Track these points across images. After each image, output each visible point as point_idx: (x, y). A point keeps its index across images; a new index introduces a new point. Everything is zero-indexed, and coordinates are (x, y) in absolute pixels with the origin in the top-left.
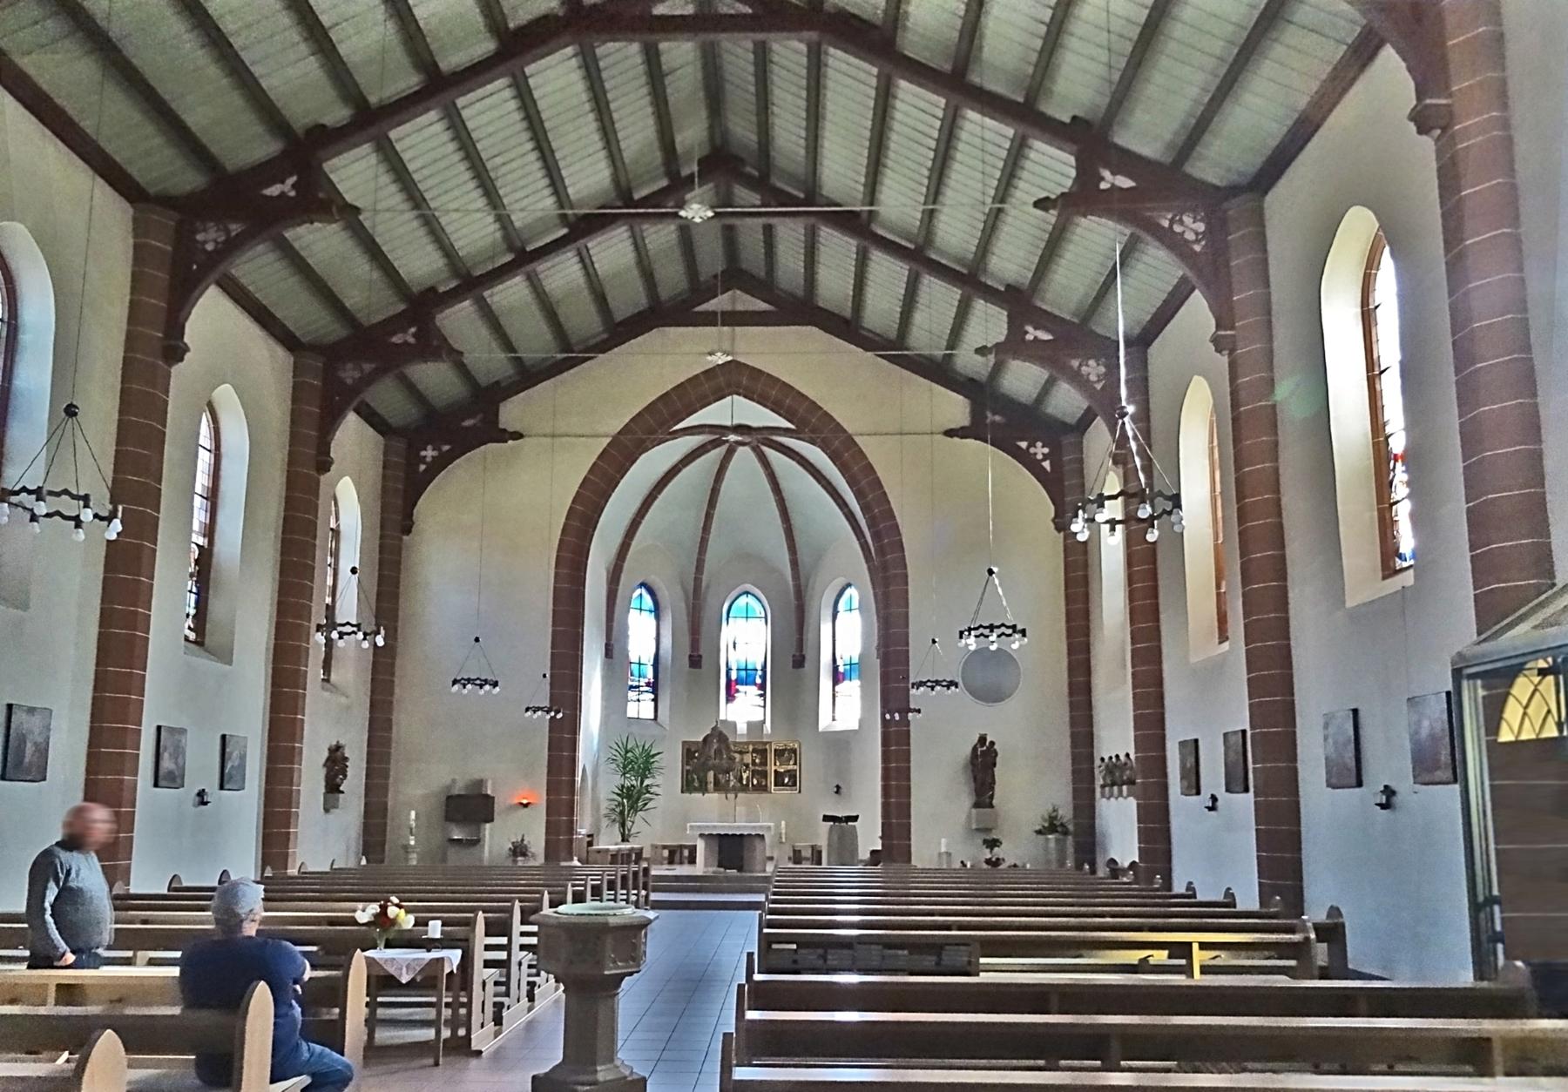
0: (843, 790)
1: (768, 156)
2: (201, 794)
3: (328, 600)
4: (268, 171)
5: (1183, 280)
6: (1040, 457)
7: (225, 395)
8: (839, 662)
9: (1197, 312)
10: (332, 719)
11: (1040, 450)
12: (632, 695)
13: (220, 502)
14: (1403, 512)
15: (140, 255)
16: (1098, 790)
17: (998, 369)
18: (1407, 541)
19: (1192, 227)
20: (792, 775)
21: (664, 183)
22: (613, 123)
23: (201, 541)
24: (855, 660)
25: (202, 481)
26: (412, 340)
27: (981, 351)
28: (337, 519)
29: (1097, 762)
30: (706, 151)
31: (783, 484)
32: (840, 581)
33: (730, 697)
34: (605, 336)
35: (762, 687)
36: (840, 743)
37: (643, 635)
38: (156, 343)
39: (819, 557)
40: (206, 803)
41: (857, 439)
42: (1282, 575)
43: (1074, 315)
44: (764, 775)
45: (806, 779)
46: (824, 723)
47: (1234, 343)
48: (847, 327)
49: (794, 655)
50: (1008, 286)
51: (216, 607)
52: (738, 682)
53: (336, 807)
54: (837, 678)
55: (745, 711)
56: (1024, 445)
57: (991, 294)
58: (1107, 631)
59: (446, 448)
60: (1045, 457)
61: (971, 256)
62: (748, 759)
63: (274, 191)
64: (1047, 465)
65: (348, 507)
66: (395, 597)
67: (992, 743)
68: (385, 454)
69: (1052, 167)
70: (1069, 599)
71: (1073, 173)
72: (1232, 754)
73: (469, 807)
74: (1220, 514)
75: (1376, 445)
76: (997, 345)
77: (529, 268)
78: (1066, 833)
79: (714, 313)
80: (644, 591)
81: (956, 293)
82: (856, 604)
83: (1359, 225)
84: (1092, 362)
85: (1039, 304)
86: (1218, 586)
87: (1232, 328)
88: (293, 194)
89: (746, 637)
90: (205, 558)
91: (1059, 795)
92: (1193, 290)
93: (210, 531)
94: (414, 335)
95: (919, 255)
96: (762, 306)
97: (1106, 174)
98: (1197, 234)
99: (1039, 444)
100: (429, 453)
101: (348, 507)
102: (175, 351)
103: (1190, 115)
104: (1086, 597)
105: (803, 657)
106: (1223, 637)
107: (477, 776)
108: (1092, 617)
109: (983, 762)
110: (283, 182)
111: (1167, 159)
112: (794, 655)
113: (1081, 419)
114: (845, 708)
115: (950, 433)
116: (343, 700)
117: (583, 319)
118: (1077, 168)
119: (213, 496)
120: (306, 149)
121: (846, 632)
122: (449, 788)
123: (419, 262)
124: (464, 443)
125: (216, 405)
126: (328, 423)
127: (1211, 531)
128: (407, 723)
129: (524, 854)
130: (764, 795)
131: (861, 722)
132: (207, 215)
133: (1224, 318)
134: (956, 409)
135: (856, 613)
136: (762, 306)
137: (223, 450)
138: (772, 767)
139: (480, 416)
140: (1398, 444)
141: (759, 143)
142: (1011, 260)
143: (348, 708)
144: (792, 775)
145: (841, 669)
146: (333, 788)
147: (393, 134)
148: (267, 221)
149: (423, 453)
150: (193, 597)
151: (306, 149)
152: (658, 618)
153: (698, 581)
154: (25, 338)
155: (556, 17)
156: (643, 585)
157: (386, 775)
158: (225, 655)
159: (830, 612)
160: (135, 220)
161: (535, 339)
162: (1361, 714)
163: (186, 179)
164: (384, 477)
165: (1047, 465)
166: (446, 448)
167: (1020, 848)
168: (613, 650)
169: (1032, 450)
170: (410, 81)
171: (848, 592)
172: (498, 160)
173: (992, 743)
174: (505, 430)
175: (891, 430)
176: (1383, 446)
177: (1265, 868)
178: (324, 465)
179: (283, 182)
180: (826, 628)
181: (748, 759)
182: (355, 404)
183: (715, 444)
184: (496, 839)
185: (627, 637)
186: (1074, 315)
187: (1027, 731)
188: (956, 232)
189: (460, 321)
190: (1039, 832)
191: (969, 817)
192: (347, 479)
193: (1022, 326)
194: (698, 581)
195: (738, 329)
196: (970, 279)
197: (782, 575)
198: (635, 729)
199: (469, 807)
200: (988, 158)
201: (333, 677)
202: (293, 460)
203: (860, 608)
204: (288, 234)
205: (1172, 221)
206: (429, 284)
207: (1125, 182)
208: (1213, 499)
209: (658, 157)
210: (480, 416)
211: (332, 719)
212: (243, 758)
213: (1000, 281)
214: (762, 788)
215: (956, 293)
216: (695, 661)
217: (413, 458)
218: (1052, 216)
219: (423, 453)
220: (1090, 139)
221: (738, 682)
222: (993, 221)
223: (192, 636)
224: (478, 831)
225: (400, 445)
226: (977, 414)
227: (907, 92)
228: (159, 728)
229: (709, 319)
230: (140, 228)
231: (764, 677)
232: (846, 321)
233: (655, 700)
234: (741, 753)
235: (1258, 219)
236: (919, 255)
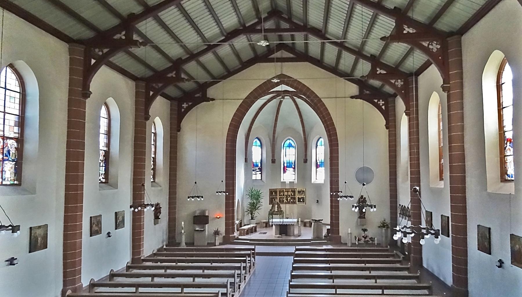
0: (319, 202)
1: (290, 10)
2: (109, 233)
3: (153, 156)
4: (116, 30)
6: (381, 105)
7: (111, 101)
8: (318, 161)
10: (155, 194)
11: (381, 103)
12: (253, 172)
13: (111, 135)
14: (510, 160)
15: (72, 61)
16: (398, 215)
18: (511, 170)
19: (435, 47)
20: (303, 199)
21: (256, 20)
22: (237, 4)
23: (105, 149)
24: (323, 161)
25: (103, 128)
26: (174, 76)
28: (155, 130)
29: (398, 206)
30: (270, 9)
31: (300, 106)
32: (318, 137)
33: (284, 172)
34: (240, 66)
35: (294, 168)
36: (318, 187)
37: (257, 154)
38: (80, 90)
39: (312, 128)
40: (110, 236)
41: (322, 99)
42: (464, 171)
43: (393, 65)
44: (295, 198)
45: (307, 200)
46: (313, 180)
47: (450, 89)
48: (319, 62)
49: (304, 158)
50: (371, 55)
51: (112, 170)
52: (287, 167)
53: (158, 223)
54: (317, 166)
55: (289, 177)
56: (376, 101)
57: (365, 58)
58: (402, 166)
59: (190, 104)
60: (383, 105)
61: (359, 46)
62: (289, 193)
63: (169, 75)
64: (383, 107)
65: (158, 126)
66: (176, 153)
67: (365, 198)
68: (171, 106)
70: (390, 151)
71: (394, 24)
72: (444, 222)
73: (201, 219)
74: (442, 137)
75: (500, 135)
77: (213, 50)
78: (388, 228)
79: (274, 58)
80: (257, 140)
81: (354, 57)
82: (323, 144)
83: (497, 56)
84: (399, 81)
85: (382, 61)
86: (440, 162)
87: (449, 84)
89: (289, 155)
90: (107, 154)
91: (385, 214)
93: (108, 145)
94: (175, 74)
95: (341, 46)
96: (292, 56)
99: (381, 100)
100: (185, 105)
101: (158, 126)
102: (86, 94)
103: (436, 9)
104: (395, 141)
105: (307, 160)
106: (441, 179)
107: (203, 208)
108: (397, 162)
109: (362, 202)
110: (120, 34)
111: (427, 22)
112: (304, 158)
114: (320, 176)
115: (352, 97)
116: (159, 188)
117: (233, 62)
118: (395, 22)
119: (109, 134)
120: (128, 22)
121: (320, 152)
122: (195, 212)
123: (175, 51)
124: (196, 102)
125: (108, 103)
126: (149, 101)
127: (438, 142)
128: (182, 192)
129: (218, 234)
130: (295, 205)
131: (325, 181)
132: (93, 48)
134: (354, 89)
135: (323, 146)
136: (292, 56)
137: (111, 117)
138: (297, 196)
139: (201, 93)
140: (509, 135)
141: (287, 7)
142: (373, 46)
143: (161, 190)
144: (303, 199)
145: (319, 164)
146: (157, 217)
147: (159, 14)
149: (183, 105)
150: (104, 168)
152: (261, 148)
153: (274, 137)
154: (29, 98)
156: (257, 138)
157: (175, 208)
158: (115, 186)
159: (315, 146)
160: (69, 49)
161: (216, 68)
162: (491, 231)
164: (171, 113)
165: (383, 107)
166: (190, 104)
167: (373, 231)
168: (247, 159)
169: (379, 102)
171: (321, 139)
172: (198, 19)
173: (365, 198)
174: (209, 98)
175: (332, 96)
176: (503, 134)
177: (455, 269)
179: (120, 34)
180: (314, 151)
181: (289, 193)
183: (277, 96)
184: (209, 229)
185: (252, 155)
186: (393, 65)
187: (376, 191)
189: (192, 67)
190: (379, 227)
191: (357, 221)
192: (158, 118)
194: (274, 137)
195: (283, 63)
196: (359, 53)
197: (300, 134)
198: (255, 184)
199: (201, 219)
200: (364, 24)
201: (156, 180)
203: (324, 145)
206: (179, 57)
208: (439, 132)
209: (254, 13)
210: (201, 93)
211: (155, 194)
212: (123, 218)
213: (369, 53)
214: (294, 203)
215: (354, 57)
216: (273, 161)
217: (180, 107)
219: (183, 105)
221: (287, 167)
223: (104, 180)
224: (204, 227)
225: (176, 103)
226: (361, 91)
228: (91, 217)
229: (272, 60)
230: (71, 52)
231: (295, 165)
232: (319, 61)
233: (261, 174)
234: (287, 192)
235: (459, 44)
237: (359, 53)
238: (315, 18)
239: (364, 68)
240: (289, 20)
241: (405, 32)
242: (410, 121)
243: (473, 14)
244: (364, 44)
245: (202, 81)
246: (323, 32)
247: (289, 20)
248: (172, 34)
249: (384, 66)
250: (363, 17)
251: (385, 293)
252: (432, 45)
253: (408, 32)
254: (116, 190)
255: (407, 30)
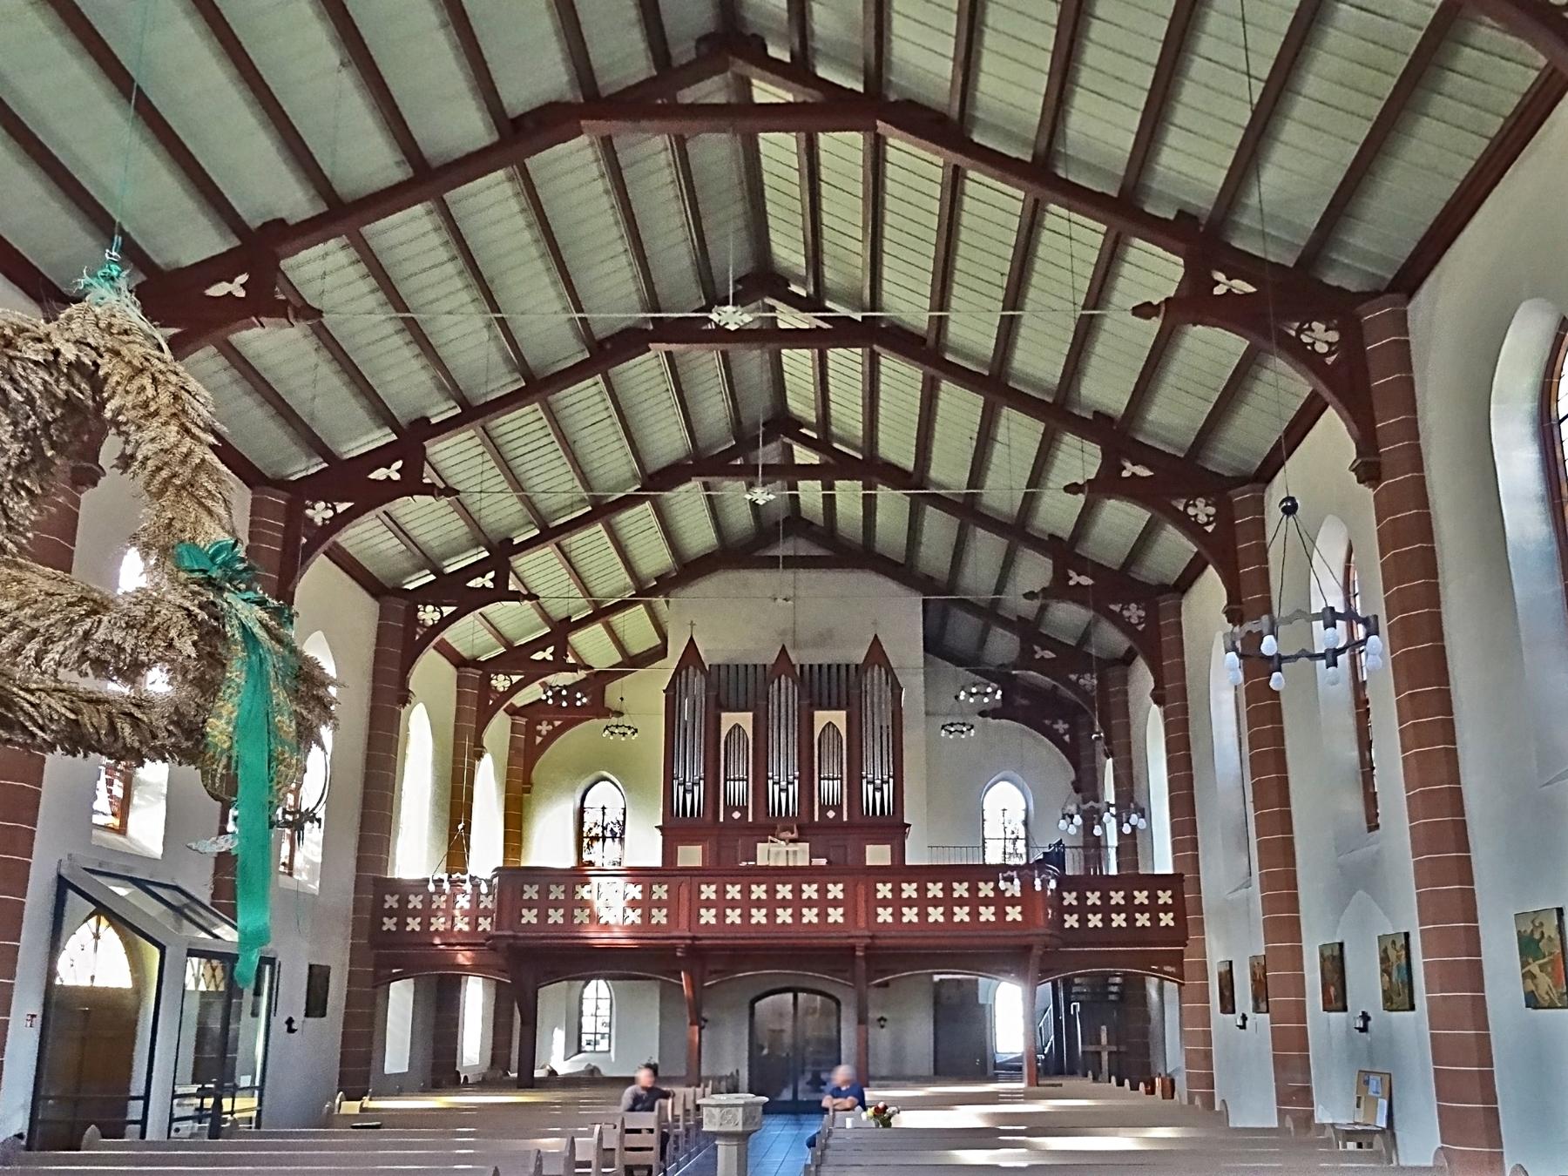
5: (1314, 396)
9: (1332, 435)
17: (1043, 609)
26: (490, 585)
27: (1030, 595)
57: (1006, 624)
63: (218, 290)
64: (1067, 738)
69: (1154, 271)
76: (1044, 589)
88: (242, 294)
92: (1205, 567)
95: (996, 384)
96: (817, 552)
97: (1128, 464)
98: (1330, 344)
100: (544, 728)
110: (231, 282)
113: (1266, 461)
133: (1367, 440)
142: (1105, 387)
148: (372, 497)
151: (261, 247)
155: (568, 105)
163: (305, 467)
165: (1067, 738)
169: (1126, 613)
170: (507, 383)
178: (404, 698)
182: (325, 547)
188: (1039, 358)
193: (1118, 460)
196: (1059, 412)
202: (376, 693)
204: (234, 338)
205: (1187, 506)
207: (1242, 286)
217: (531, 731)
218: (1081, 498)
220: (1202, 238)
222: (1085, 332)
227: (949, 392)
229: (772, 563)
232: (922, 340)
236: (996, 384)
237: (1018, 530)
238: (923, 55)
239: (1003, 645)
240: (798, 70)
241: (1125, 474)
242: (1166, 716)
243: (1477, 156)
244: (1030, 501)
245: (558, 610)
246: (931, 342)
247: (798, 70)
248: (333, 345)
249: (1144, 454)
250: (1067, 263)
251: (139, 1118)
252: (1195, 506)
253: (1134, 474)
254: (314, 962)
255: (1223, 284)
